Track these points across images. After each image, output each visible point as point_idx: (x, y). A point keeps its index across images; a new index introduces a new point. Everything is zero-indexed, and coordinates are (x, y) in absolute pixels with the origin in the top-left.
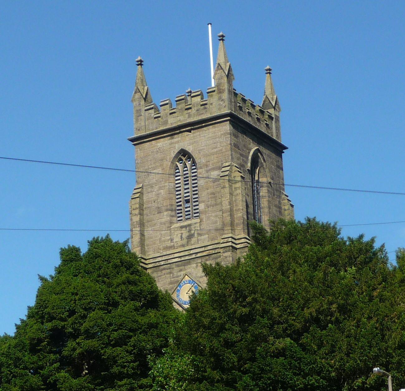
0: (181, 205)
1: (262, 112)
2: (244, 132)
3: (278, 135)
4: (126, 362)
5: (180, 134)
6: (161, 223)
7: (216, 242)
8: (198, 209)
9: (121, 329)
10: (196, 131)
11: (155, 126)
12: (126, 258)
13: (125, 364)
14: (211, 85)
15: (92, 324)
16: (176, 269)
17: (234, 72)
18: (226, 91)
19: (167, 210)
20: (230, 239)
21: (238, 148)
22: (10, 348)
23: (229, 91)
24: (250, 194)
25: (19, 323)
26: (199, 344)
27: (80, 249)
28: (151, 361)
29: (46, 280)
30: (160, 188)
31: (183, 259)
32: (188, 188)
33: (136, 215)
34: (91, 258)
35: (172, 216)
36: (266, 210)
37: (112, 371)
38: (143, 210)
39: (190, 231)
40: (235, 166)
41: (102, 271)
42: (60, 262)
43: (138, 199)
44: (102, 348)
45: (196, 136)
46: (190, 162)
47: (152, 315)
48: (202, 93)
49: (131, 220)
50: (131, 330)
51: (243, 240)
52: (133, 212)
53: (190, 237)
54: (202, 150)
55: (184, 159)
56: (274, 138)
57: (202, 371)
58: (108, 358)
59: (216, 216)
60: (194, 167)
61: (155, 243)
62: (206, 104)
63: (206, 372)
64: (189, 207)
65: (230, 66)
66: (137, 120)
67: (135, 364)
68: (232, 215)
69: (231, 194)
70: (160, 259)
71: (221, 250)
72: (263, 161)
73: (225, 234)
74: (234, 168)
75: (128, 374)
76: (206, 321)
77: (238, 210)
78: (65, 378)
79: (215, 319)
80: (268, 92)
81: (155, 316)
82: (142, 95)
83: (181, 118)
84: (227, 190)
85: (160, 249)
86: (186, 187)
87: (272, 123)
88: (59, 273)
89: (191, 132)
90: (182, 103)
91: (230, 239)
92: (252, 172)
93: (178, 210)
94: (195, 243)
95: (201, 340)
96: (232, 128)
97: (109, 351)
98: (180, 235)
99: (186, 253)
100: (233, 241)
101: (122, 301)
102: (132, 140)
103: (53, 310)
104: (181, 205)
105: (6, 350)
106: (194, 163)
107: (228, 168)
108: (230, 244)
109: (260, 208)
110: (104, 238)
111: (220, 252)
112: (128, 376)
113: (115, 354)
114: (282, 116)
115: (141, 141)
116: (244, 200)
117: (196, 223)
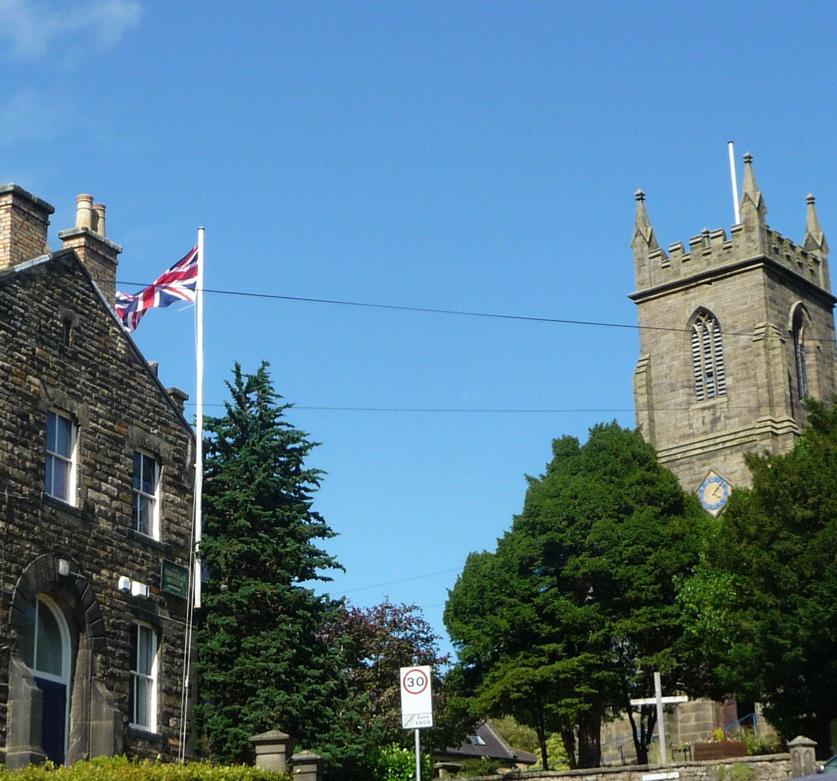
0: (701, 380)
1: (804, 254)
2: (782, 282)
3: (827, 284)
4: (645, 584)
5: (697, 288)
6: (676, 405)
7: (750, 427)
8: (724, 384)
9: (638, 544)
10: (718, 282)
11: (663, 278)
12: (639, 450)
13: (643, 587)
14: (734, 222)
15: (598, 536)
16: (698, 464)
17: (766, 203)
18: (757, 229)
19: (683, 387)
20: (769, 423)
21: (775, 302)
22: (493, 568)
23: (761, 229)
24: (793, 362)
25: (502, 537)
26: (743, 559)
27: (577, 440)
28: (678, 582)
29: (536, 480)
30: (673, 359)
31: (706, 450)
32: (710, 358)
33: (642, 394)
34: (594, 451)
35: (691, 395)
36: (815, 383)
37: (627, 595)
38: (651, 388)
39: (714, 414)
40: (773, 327)
41: (609, 467)
42: (553, 457)
43: (644, 375)
44: (612, 569)
45: (718, 289)
46: (711, 324)
47: (676, 524)
48: (724, 232)
49: (636, 401)
50: (650, 545)
51: (786, 424)
52: (638, 391)
53: (715, 421)
54: (727, 306)
55: (703, 319)
56: (822, 287)
57: (747, 594)
58: (621, 580)
59: (749, 393)
60: (717, 330)
61: (668, 431)
62: (730, 247)
63: (754, 596)
64: (712, 382)
65: (761, 197)
66: (639, 271)
67: (656, 587)
68: (770, 392)
69: (768, 363)
70: (676, 451)
71: (758, 438)
72: (808, 319)
73: (762, 416)
74: (771, 329)
75: (647, 600)
76: (752, 530)
77: (777, 384)
78: (567, 606)
79: (763, 526)
80: (811, 229)
81: (680, 525)
82: (644, 239)
83: (698, 266)
84: (763, 358)
85: (676, 438)
86: (708, 356)
87: (818, 268)
88: (553, 471)
89: (711, 284)
90: (699, 247)
91: (769, 423)
92: (794, 334)
93: (698, 386)
94: (722, 429)
95: (744, 554)
96: (766, 277)
97: (621, 571)
98: (701, 419)
99: (711, 442)
100: (773, 424)
101: (638, 506)
102: (634, 298)
103: (547, 517)
104: (701, 380)
105: (488, 570)
106: (717, 324)
107: (763, 330)
108: (769, 429)
109: (805, 381)
110: (610, 424)
111: (755, 440)
112: (648, 603)
113: (630, 574)
114: (830, 258)
115: (732, 272)
116: (786, 370)
117: (722, 403)
